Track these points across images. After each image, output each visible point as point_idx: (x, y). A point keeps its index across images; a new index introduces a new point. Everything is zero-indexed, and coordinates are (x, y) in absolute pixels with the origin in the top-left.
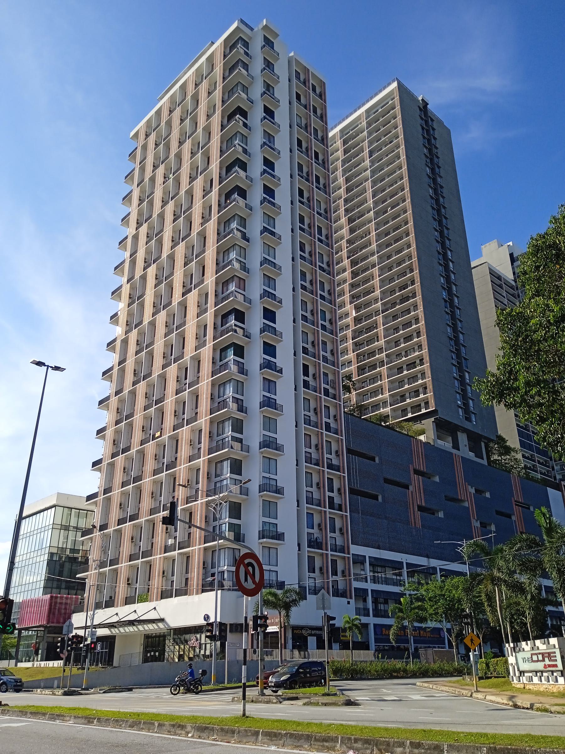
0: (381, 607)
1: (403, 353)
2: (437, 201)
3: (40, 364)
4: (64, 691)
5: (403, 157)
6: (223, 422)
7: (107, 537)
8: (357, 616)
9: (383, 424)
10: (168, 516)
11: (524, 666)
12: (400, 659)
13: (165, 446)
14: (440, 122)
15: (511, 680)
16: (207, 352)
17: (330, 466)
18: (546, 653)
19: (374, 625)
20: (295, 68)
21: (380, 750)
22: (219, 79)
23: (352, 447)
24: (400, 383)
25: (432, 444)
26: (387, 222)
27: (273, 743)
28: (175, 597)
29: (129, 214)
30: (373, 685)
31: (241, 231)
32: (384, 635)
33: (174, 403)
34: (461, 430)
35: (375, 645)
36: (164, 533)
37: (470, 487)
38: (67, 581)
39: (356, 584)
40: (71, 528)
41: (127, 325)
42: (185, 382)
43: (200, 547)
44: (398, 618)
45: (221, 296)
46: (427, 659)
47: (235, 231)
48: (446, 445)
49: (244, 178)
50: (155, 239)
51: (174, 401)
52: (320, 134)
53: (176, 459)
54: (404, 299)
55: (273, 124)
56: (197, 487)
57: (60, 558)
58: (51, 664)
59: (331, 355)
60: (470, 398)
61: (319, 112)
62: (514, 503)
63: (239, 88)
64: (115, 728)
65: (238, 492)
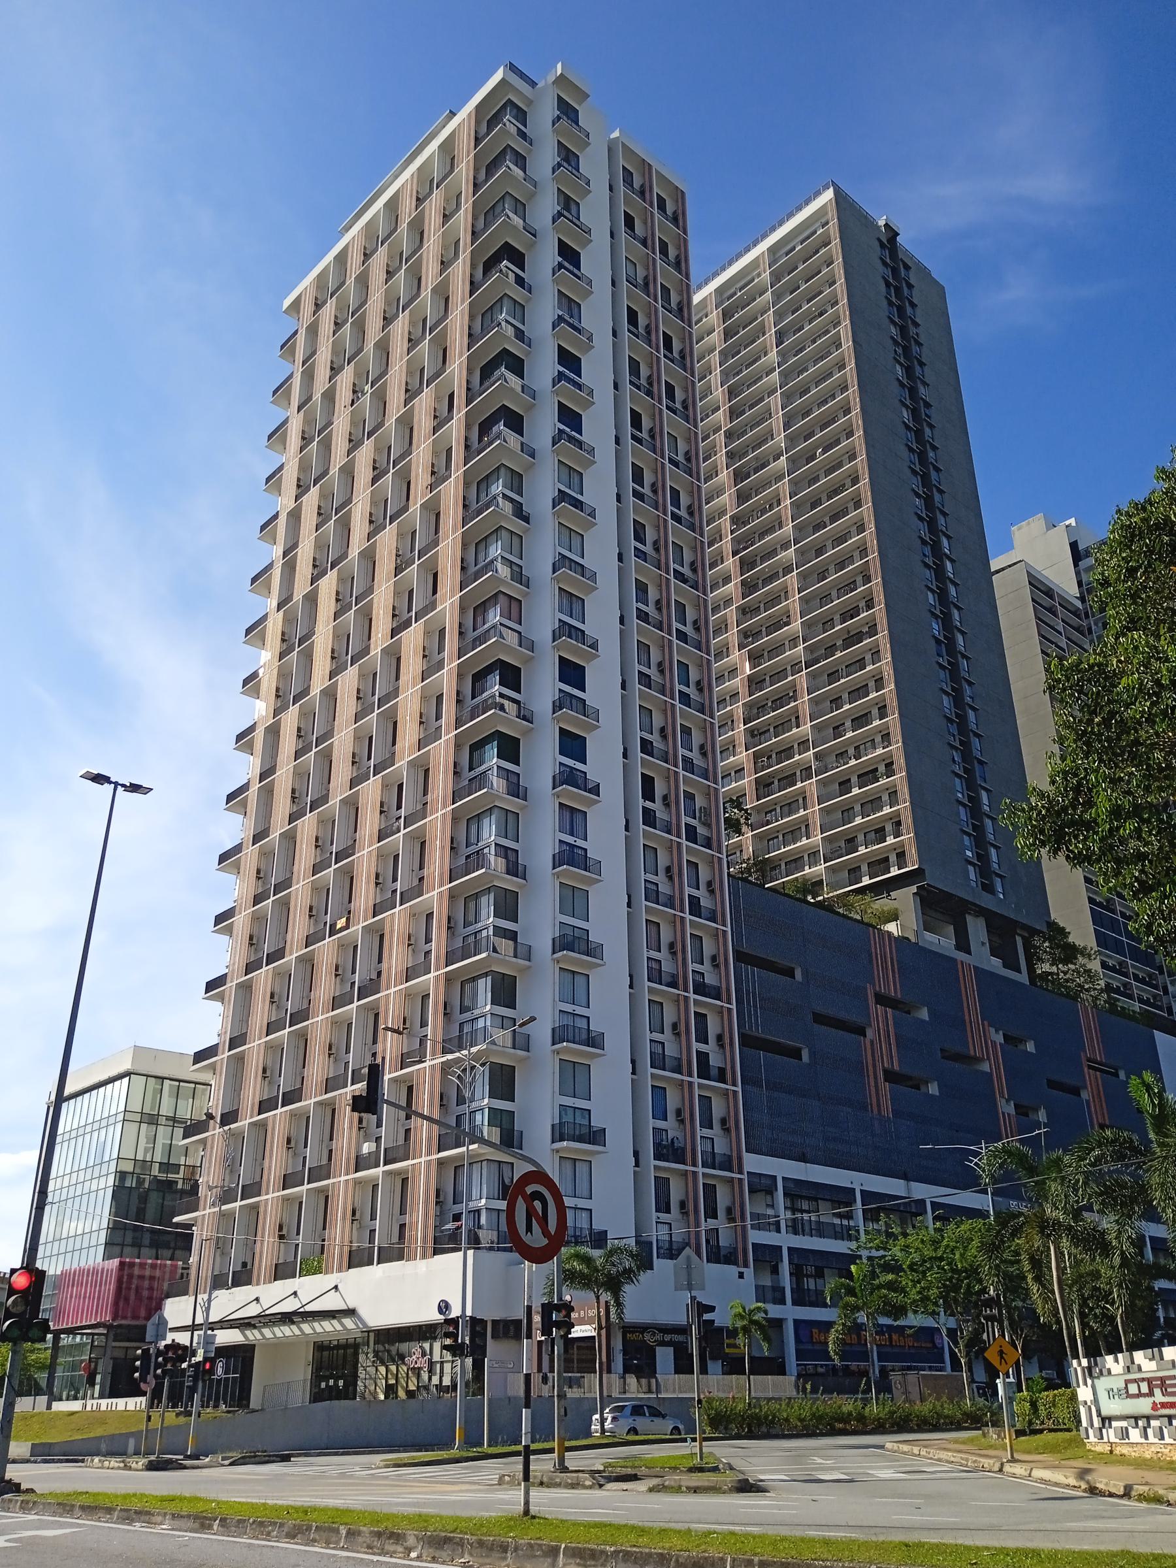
0: (810, 1284)
1: (851, 751)
2: (919, 434)
3: (99, 779)
5: (847, 344)
8: (759, 1304)
9: (809, 898)
10: (364, 1094)
11: (1110, 1407)
13: (356, 947)
14: (925, 272)
15: (1083, 1434)
16: (442, 752)
17: (700, 989)
18: (1156, 1379)
19: (795, 1321)
20: (621, 162)
22: (466, 188)
23: (745, 948)
24: (846, 814)
25: (913, 940)
26: (816, 479)
28: (378, 1263)
29: (281, 468)
31: (511, 500)
32: (817, 1343)
33: (374, 859)
35: (798, 1365)
36: (355, 1129)
37: (992, 1030)
38: (153, 1231)
39: (756, 1237)
40: (162, 1120)
41: (277, 696)
43: (429, 1158)
45: (471, 635)
47: (500, 500)
48: (943, 942)
49: (520, 389)
51: (375, 854)
52: (674, 298)
53: (379, 974)
54: (853, 638)
55: (579, 278)
56: (422, 1032)
57: (140, 1182)
58: (121, 1404)
62: (1085, 1063)
63: (506, 206)
64: (258, 1539)
65: (509, 1043)
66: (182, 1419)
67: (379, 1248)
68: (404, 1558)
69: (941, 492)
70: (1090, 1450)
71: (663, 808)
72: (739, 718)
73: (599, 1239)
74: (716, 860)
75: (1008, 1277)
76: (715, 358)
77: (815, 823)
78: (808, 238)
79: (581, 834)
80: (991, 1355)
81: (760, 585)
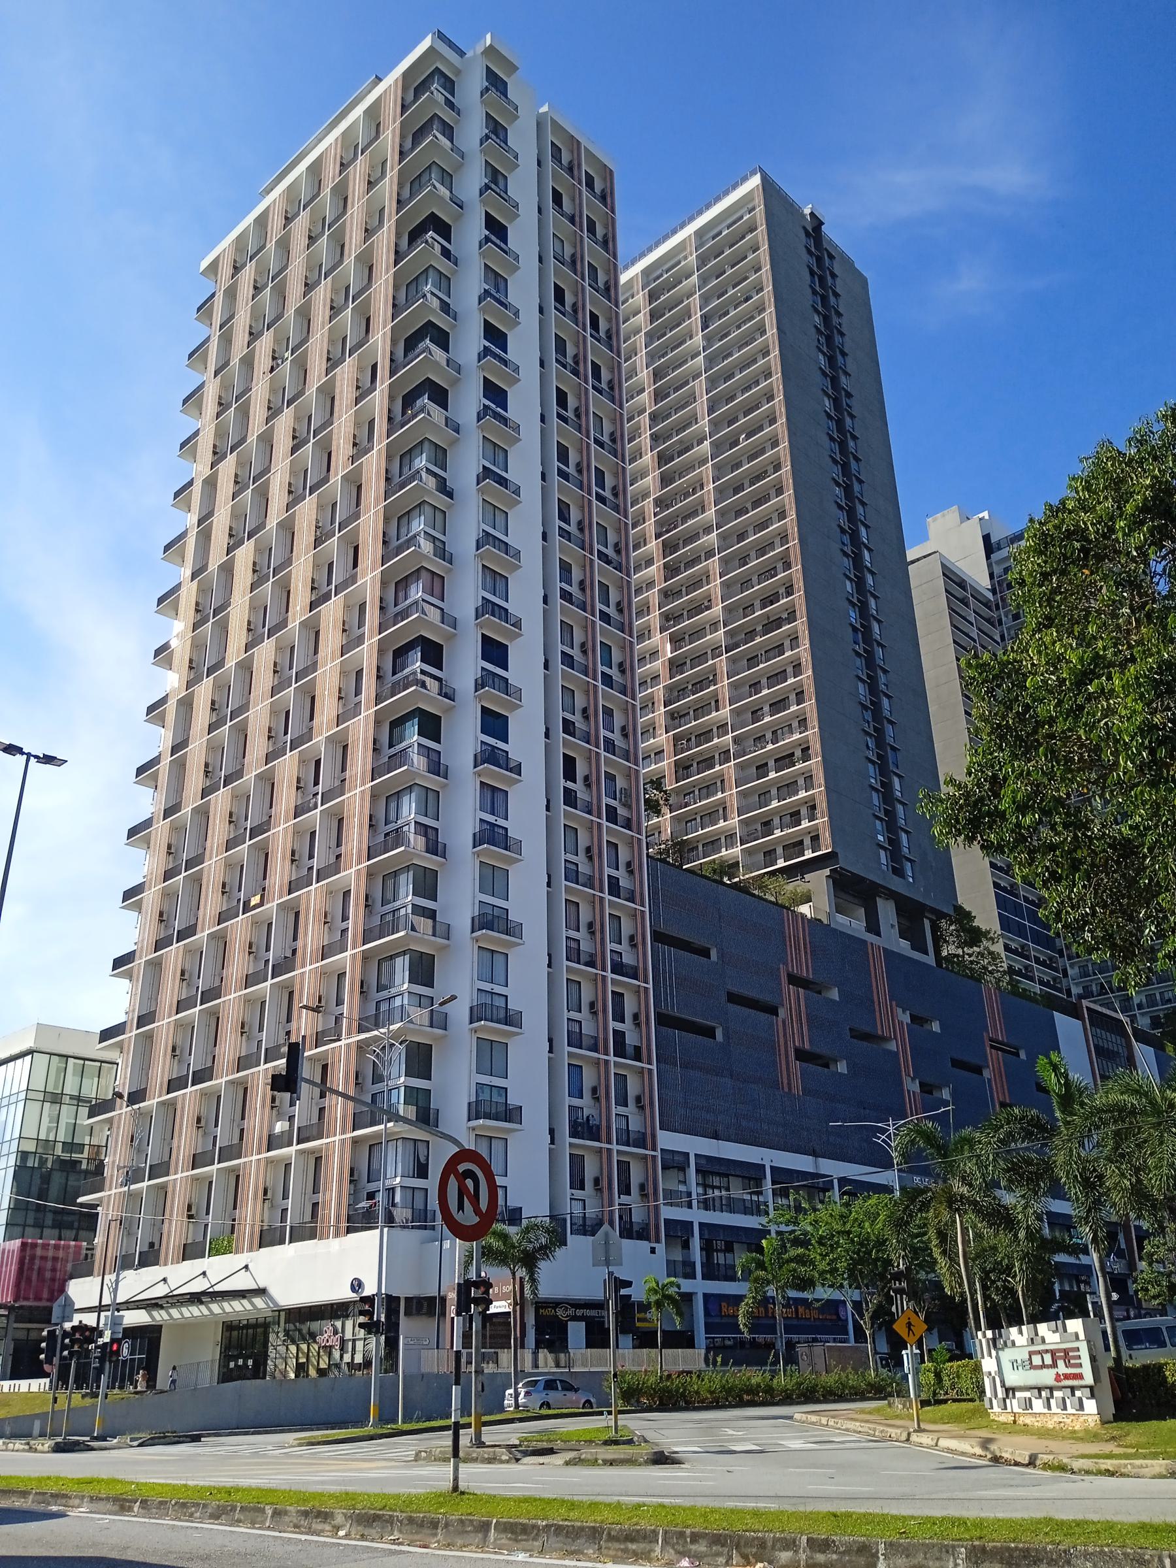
0: (720, 1258)
1: (769, 736)
2: (840, 423)
3: (11, 749)
4: (56, 1443)
5: (772, 332)
6: (396, 874)
7: (143, 1117)
8: (673, 1279)
9: (725, 880)
10: (284, 1073)
11: (1013, 1378)
12: (757, 1365)
13: (270, 924)
14: (848, 263)
15: (987, 1405)
16: (361, 728)
17: (618, 968)
18: (1059, 1350)
19: (705, 1295)
20: (550, 138)
21: (745, 1557)
22: (392, 156)
23: (662, 928)
24: (762, 797)
25: (825, 922)
26: (738, 465)
27: (520, 1546)
28: (290, 1242)
29: (196, 433)
30: (706, 1420)
31: (435, 475)
32: (725, 1316)
33: (290, 835)
34: (885, 894)
35: (706, 1338)
36: (268, 1108)
37: (900, 1010)
38: (56, 1212)
39: (669, 1213)
40: (66, 1099)
41: (191, 668)
42: (314, 790)
43: (344, 1137)
44: (756, 1280)
45: (392, 610)
46: (812, 1364)
47: (424, 474)
48: (853, 924)
49: (444, 363)
50: (251, 488)
51: (291, 830)
52: (602, 278)
53: (294, 952)
54: (772, 624)
55: (506, 252)
56: (338, 1010)
57: (43, 1162)
58: (24, 1385)
59: (621, 738)
60: (903, 830)
61: (600, 231)
62: (988, 1043)
63: (433, 176)
64: (180, 1520)
65: (426, 1022)
66: (88, 1401)
67: (291, 1227)
68: (332, 1537)
69: (861, 482)
70: (993, 1420)
71: (584, 788)
72: (659, 700)
73: (514, 1216)
74: (635, 841)
75: (915, 1251)
76: (641, 339)
77: (732, 805)
78: (734, 223)
79: (502, 813)
80: (899, 1327)
81: (682, 569)
